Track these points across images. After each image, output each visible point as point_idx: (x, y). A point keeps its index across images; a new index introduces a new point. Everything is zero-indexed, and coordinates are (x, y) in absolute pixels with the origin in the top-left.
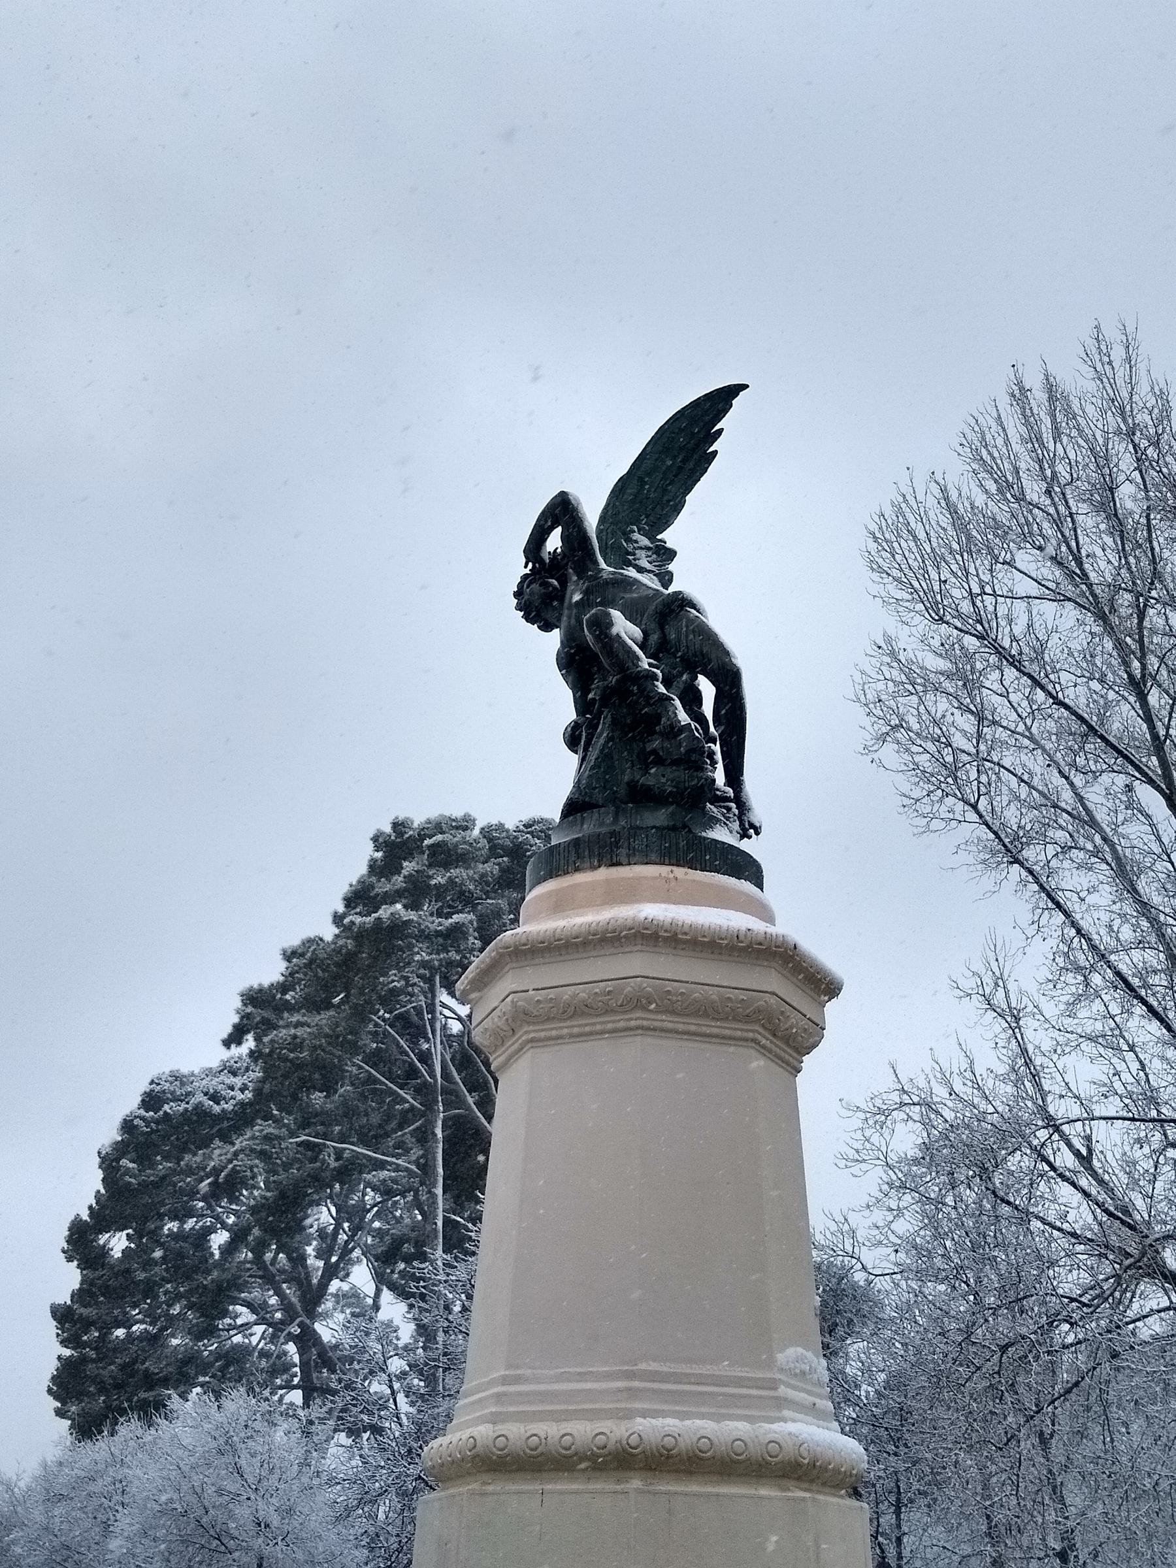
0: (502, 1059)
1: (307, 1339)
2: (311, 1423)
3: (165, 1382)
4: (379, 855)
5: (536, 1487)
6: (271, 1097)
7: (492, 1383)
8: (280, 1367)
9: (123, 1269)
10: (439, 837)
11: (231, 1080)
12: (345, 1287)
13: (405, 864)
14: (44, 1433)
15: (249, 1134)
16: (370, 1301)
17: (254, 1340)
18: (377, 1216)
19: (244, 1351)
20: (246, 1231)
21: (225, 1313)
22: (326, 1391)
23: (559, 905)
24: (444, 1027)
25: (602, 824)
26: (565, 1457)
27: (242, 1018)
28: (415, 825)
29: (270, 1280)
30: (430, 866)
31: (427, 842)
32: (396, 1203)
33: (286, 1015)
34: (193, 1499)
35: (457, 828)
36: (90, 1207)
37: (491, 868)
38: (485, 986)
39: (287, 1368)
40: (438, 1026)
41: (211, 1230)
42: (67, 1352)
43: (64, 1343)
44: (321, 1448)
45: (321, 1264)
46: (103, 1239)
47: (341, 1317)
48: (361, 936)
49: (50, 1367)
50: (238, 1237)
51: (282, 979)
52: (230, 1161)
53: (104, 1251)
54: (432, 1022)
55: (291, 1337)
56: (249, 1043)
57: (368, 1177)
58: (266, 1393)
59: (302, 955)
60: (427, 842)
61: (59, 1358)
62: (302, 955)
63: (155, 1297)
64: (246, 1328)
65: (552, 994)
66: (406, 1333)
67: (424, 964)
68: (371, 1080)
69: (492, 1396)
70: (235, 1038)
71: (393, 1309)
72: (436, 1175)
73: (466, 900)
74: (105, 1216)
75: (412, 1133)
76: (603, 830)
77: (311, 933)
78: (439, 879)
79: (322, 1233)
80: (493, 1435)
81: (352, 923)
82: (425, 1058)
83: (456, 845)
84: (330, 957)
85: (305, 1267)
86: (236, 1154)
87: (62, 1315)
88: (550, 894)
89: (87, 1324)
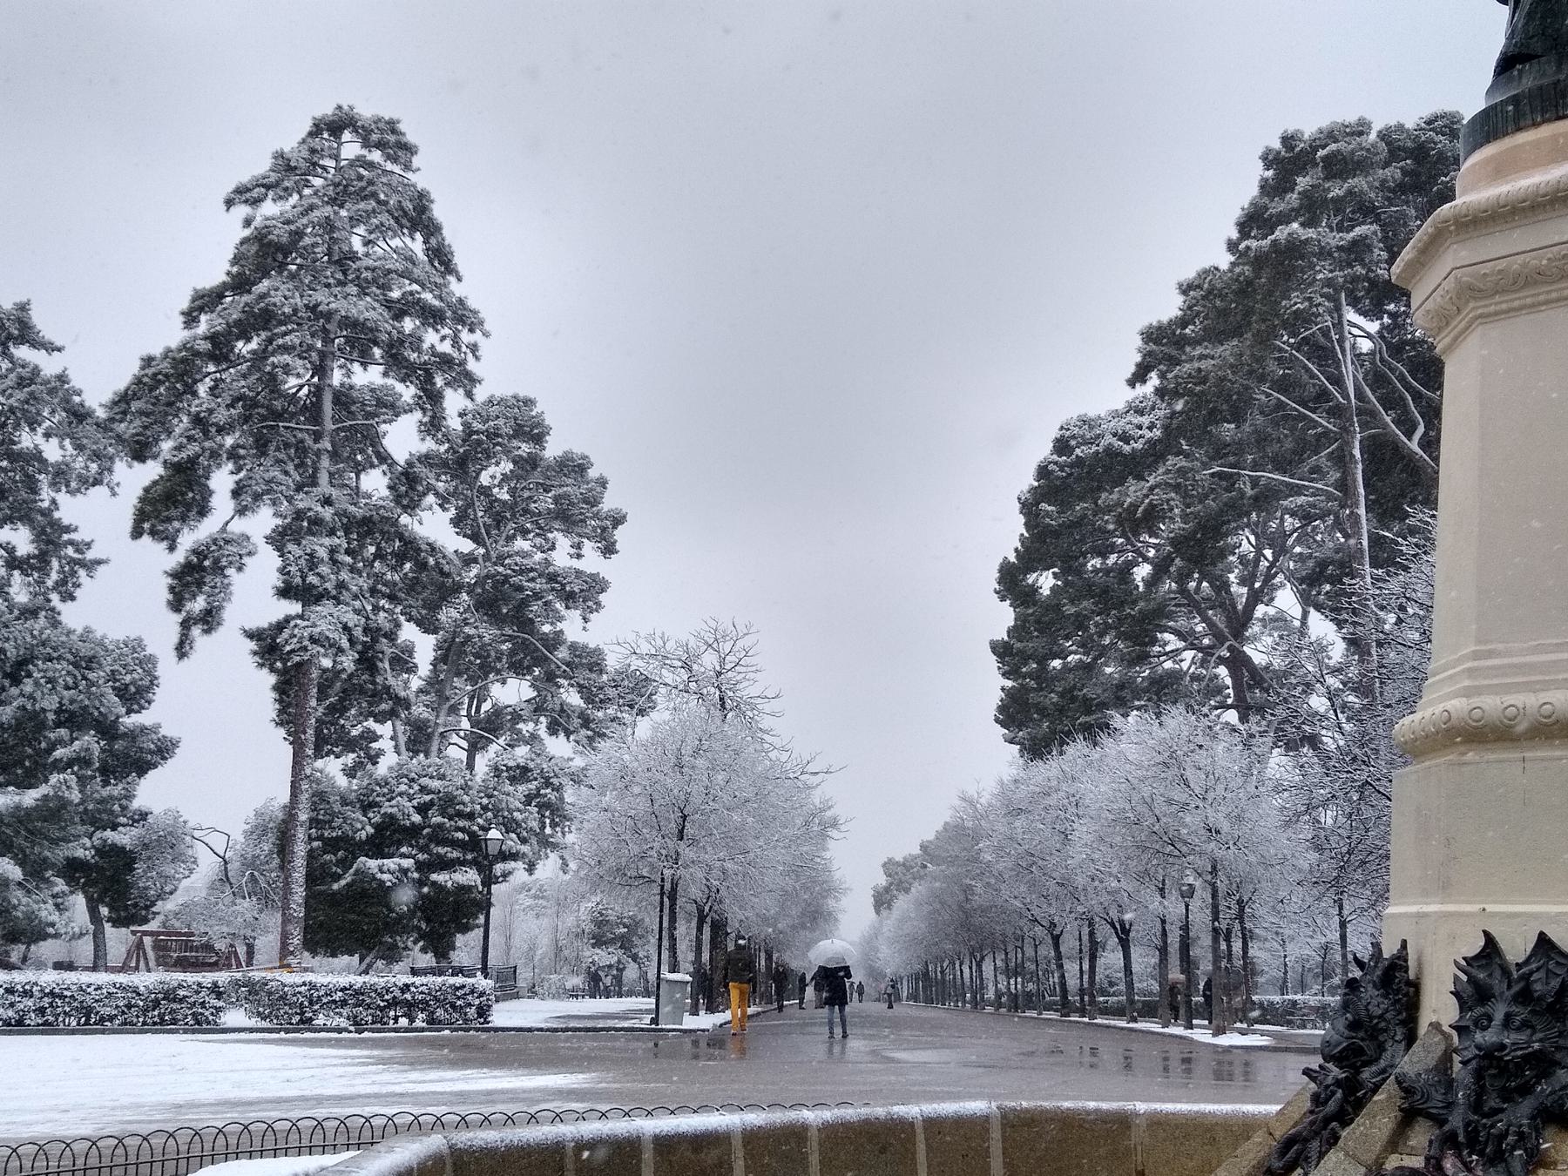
0: (1448, 340)
1: (1238, 663)
2: (1252, 736)
3: (1103, 705)
4: (1270, 173)
5: (1518, 755)
6: (1181, 431)
7: (1460, 661)
8: (1216, 690)
9: (1053, 604)
10: (1333, 147)
11: (1138, 420)
12: (1271, 611)
13: (1299, 180)
14: (994, 760)
15: (1161, 471)
16: (1297, 624)
17: (1185, 666)
18: (1298, 541)
19: (1176, 676)
20: (1168, 560)
21: (1154, 641)
22: (1261, 710)
23: (1499, 170)
24: (1353, 347)
25: (1544, 75)
26: (1546, 725)
27: (1144, 356)
28: (1306, 137)
29: (1194, 605)
30: (1327, 178)
31: (1321, 153)
32: (1315, 528)
33: (1188, 349)
34: (1145, 809)
35: (1352, 134)
36: (1016, 550)
37: (1393, 173)
38: (1423, 265)
39: (1220, 690)
40: (1347, 346)
41: (1135, 564)
42: (1009, 684)
43: (1005, 675)
44: (1262, 760)
45: (1245, 590)
46: (1031, 578)
47: (1269, 640)
48: (1259, 261)
49: (995, 697)
50: (1161, 569)
51: (1180, 313)
52: (1146, 496)
53: (1034, 590)
54: (1341, 341)
55: (1222, 661)
56: (1154, 380)
57: (1285, 503)
58: (1205, 710)
59: (1199, 287)
60: (1321, 153)
61: (1003, 689)
62: (1199, 287)
63: (1086, 629)
64: (1176, 653)
65: (1502, 264)
66: (1337, 651)
67: (1329, 283)
68: (1280, 405)
69: (1463, 671)
70: (1139, 377)
71: (1321, 627)
72: (1356, 494)
73: (1367, 211)
74: (1033, 554)
75: (1330, 457)
76: (1545, 81)
77: (1207, 264)
78: (1336, 191)
79: (1243, 559)
80: (1467, 708)
81: (1248, 248)
82: (1338, 381)
83: (1353, 152)
84: (1228, 286)
85: (1228, 592)
86: (1152, 489)
87: (1001, 650)
88: (1487, 161)
89: (1025, 658)
